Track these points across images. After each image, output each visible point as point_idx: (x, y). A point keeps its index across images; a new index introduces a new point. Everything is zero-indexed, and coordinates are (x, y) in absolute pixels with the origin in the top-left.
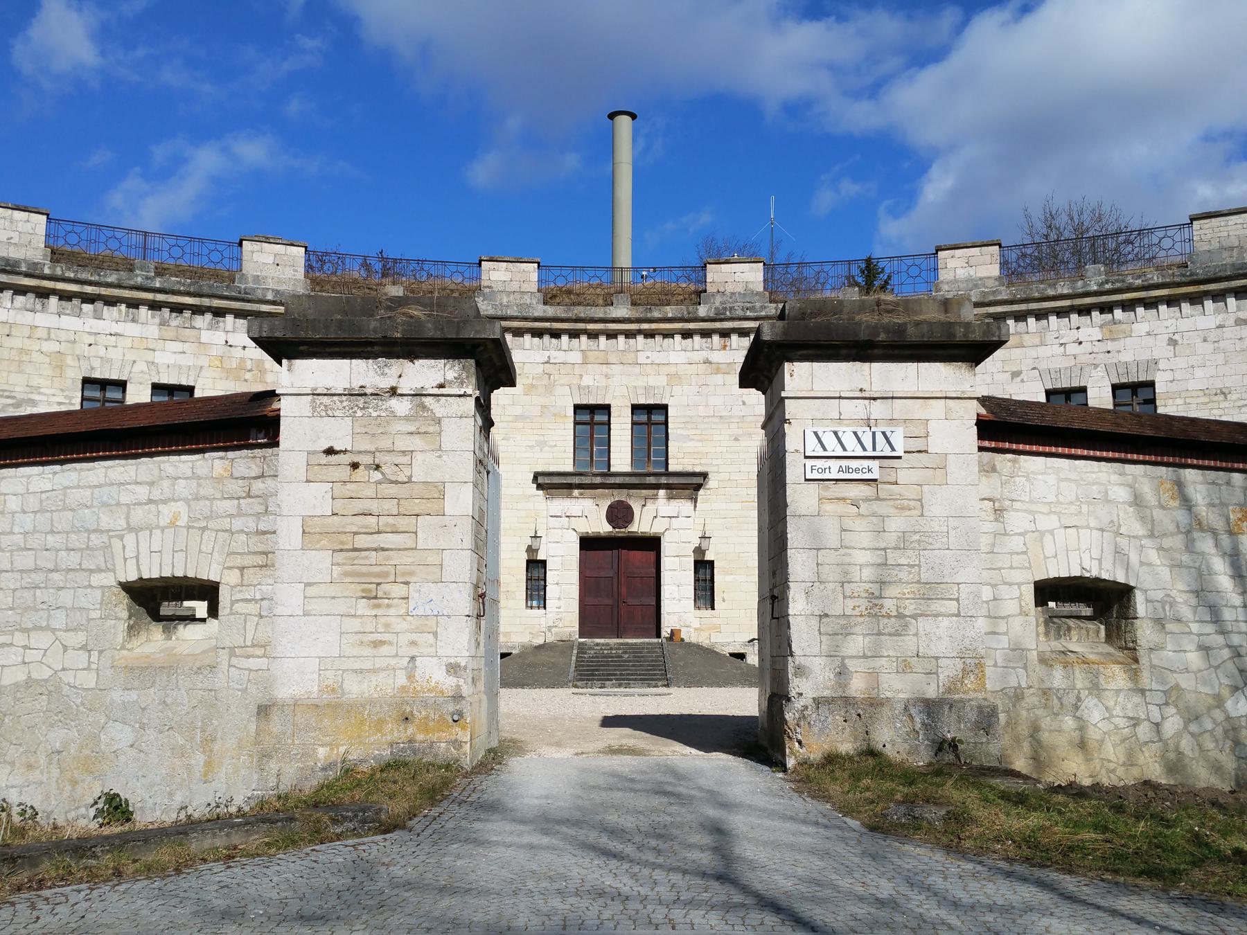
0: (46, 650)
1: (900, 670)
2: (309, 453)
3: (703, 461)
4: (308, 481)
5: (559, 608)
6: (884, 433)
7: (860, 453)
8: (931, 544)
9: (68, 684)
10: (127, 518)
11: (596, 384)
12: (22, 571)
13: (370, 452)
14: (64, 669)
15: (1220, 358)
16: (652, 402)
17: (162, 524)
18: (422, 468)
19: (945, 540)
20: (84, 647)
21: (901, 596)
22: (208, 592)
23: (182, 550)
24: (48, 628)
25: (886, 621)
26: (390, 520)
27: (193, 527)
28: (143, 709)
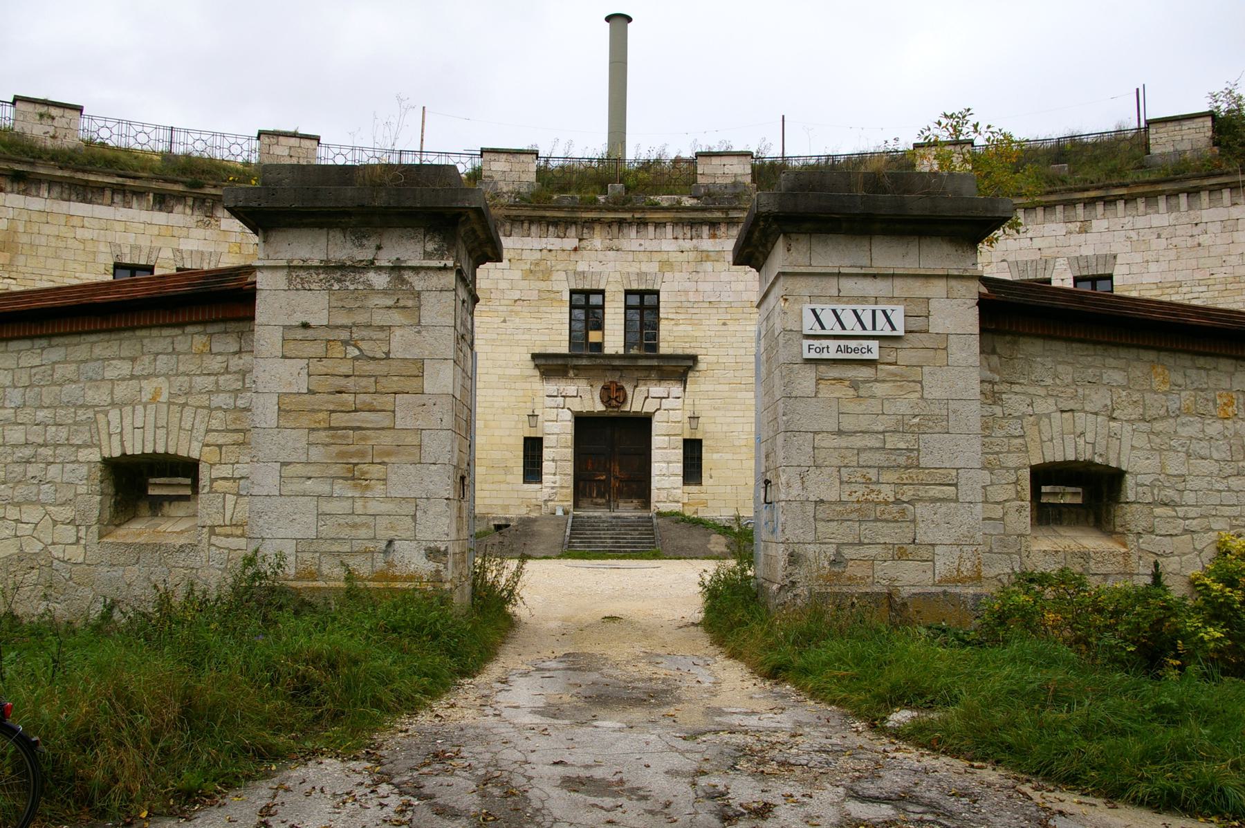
0: (37, 524)
1: (896, 557)
2: (285, 327)
3: (692, 345)
4: (284, 357)
5: (555, 483)
6: (884, 312)
7: (858, 331)
8: (930, 428)
9: (58, 559)
10: (112, 393)
11: (591, 270)
12: (13, 446)
13: (346, 327)
14: (53, 543)
15: (1172, 254)
16: (643, 287)
17: (144, 400)
18: (401, 343)
19: (944, 423)
20: (72, 522)
21: (899, 481)
22: (188, 468)
23: (163, 427)
24: (37, 502)
25: (883, 508)
26: (367, 398)
27: (174, 404)
28: (129, 585)
